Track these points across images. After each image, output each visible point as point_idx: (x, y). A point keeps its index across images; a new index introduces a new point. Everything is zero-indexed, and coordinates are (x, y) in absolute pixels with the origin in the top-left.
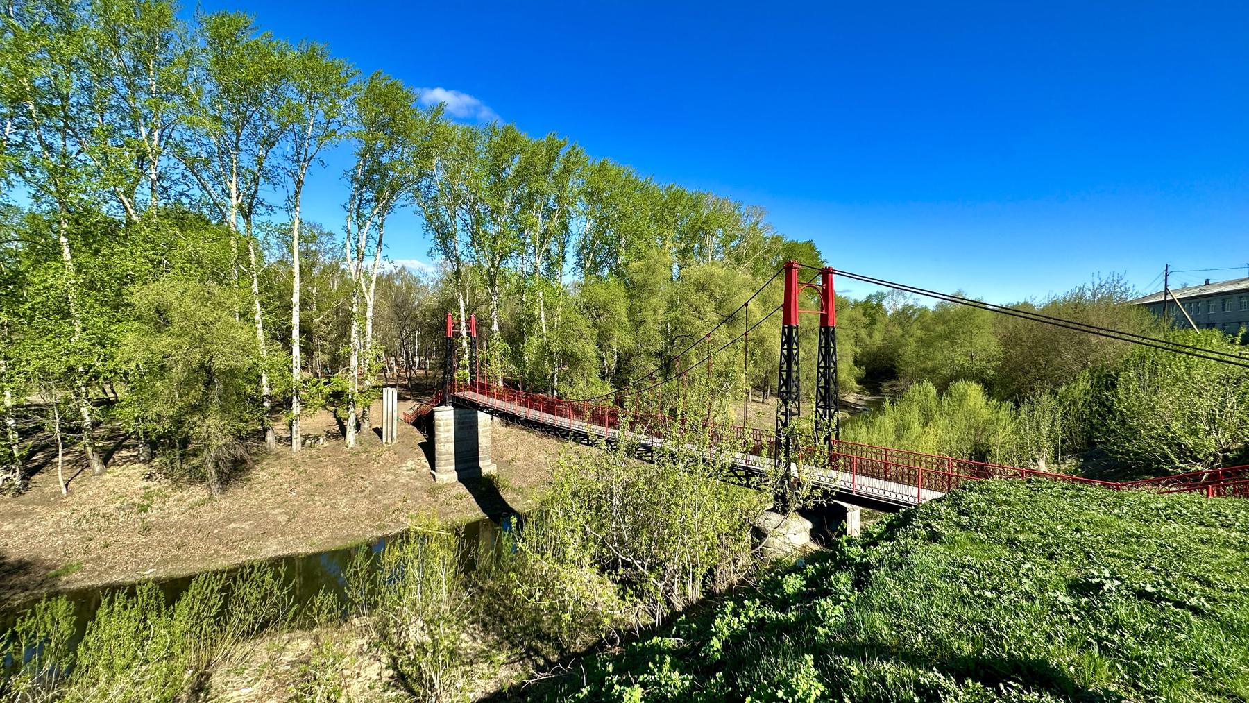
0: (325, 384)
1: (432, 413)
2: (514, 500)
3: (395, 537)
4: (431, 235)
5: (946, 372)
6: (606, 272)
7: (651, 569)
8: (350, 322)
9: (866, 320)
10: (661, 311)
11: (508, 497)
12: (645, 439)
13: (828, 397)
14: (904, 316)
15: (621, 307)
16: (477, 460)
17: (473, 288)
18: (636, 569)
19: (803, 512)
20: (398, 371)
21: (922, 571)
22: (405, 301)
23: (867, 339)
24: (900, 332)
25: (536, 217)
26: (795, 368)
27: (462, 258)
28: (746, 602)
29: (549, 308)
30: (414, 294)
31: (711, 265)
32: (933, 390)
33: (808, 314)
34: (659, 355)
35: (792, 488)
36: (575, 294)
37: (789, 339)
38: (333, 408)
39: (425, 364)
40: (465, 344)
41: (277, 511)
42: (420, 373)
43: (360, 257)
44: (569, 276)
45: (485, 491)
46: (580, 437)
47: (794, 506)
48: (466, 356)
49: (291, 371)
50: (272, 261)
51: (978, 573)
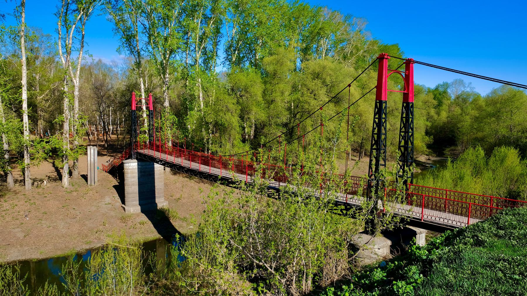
0: (47, 142)
1: (122, 164)
2: (181, 226)
3: (98, 249)
4: (119, 36)
5: (492, 140)
6: (247, 64)
7: (276, 270)
8: (63, 99)
9: (435, 102)
10: (287, 93)
11: (176, 224)
12: (274, 183)
13: (407, 157)
14: (462, 100)
15: (258, 90)
16: (154, 198)
17: (151, 76)
18: (266, 269)
19: (386, 234)
20: (98, 135)
21: (470, 263)
22: (102, 85)
23: (436, 117)
24: (460, 111)
25: (196, 23)
26: (383, 131)
27: (142, 53)
28: (344, 287)
29: (205, 91)
30: (108, 80)
31: (324, 61)
32: (482, 153)
33: (394, 100)
34: (285, 125)
35: (379, 217)
36: (224, 81)
37: (380, 110)
38: (52, 161)
39: (117, 130)
40: (145, 116)
41: (17, 230)
42: (114, 137)
43: (68, 53)
44: (220, 67)
45: (160, 220)
46: (227, 182)
47: (379, 228)
48: (146, 125)
49: (22, 133)
50: (8, 55)
51: (510, 264)
